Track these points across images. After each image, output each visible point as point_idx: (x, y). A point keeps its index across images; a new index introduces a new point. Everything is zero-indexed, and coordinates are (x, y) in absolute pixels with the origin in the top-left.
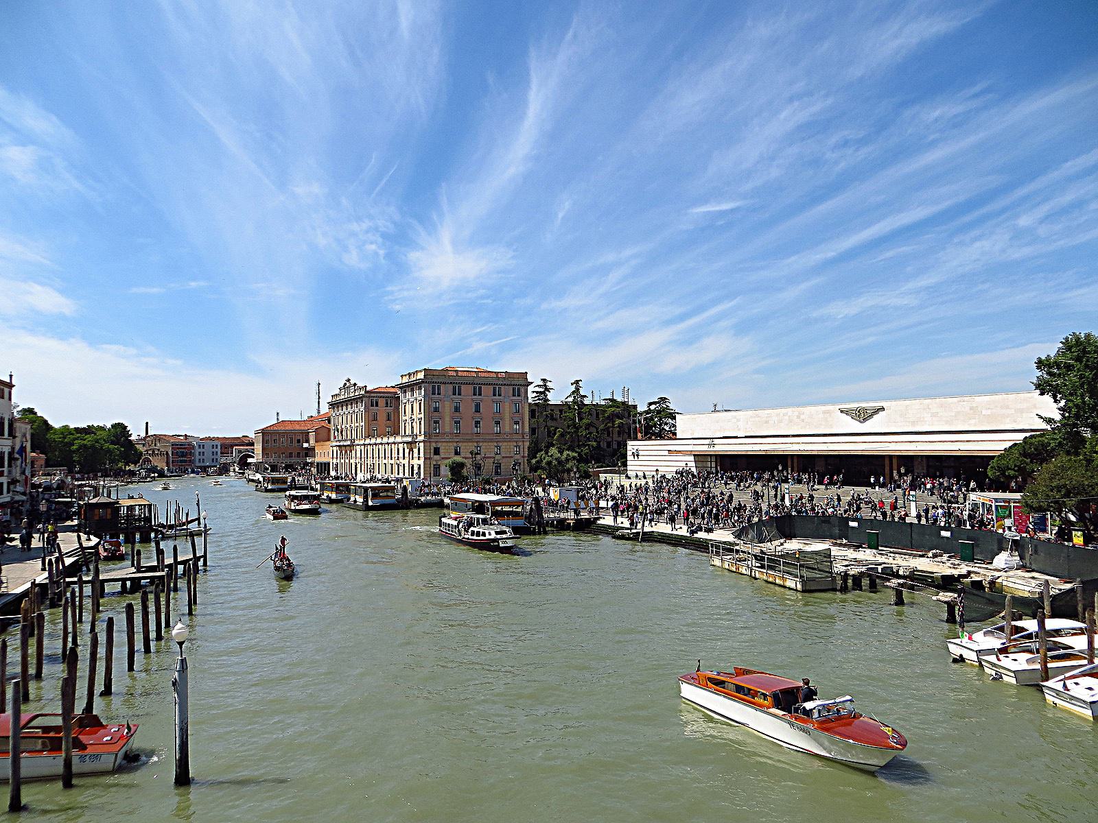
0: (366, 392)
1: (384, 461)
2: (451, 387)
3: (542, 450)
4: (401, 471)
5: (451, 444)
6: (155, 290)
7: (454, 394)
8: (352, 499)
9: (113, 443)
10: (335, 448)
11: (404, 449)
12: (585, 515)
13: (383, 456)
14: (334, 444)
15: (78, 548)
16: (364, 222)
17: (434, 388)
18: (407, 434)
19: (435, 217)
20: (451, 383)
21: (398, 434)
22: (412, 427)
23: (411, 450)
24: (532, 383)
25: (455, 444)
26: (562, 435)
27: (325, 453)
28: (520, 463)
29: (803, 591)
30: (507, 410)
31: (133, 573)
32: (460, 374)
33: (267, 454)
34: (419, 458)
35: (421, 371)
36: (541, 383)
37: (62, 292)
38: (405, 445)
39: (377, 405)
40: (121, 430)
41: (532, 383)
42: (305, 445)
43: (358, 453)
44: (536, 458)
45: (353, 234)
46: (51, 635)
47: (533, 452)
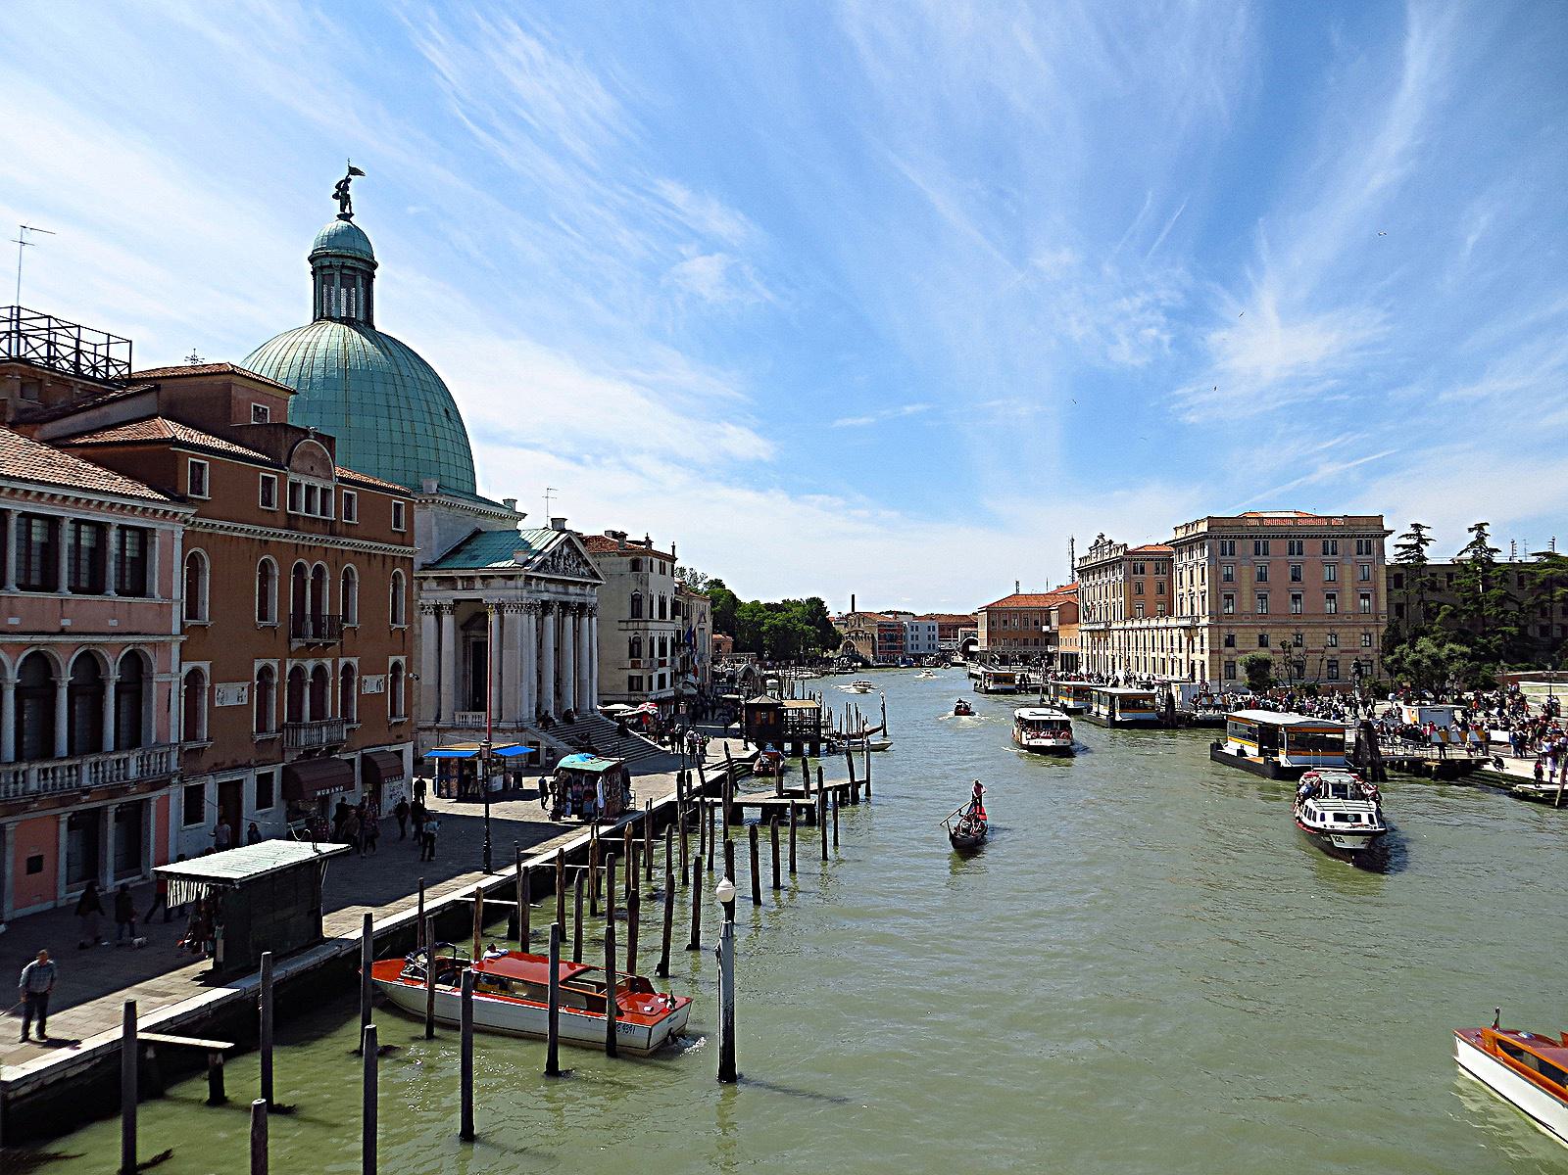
0: (1126, 553)
1: (1153, 655)
2: (1252, 542)
3: (1404, 642)
4: (1177, 669)
5: (1253, 630)
6: (863, 421)
7: (1257, 553)
8: (1095, 709)
9: (808, 623)
10: (1084, 633)
11: (1180, 638)
12: (1459, 754)
13: (1151, 646)
14: (1083, 627)
15: (724, 762)
16: (1138, 296)
17: (1223, 545)
18: (1184, 615)
19: (1249, 274)
20: (1251, 537)
21: (1171, 614)
22: (1192, 605)
23: (1191, 639)
24: (1391, 532)
25: (1259, 631)
26: (1452, 615)
27: (1072, 640)
28: (1372, 661)
30: (1348, 576)
31: (775, 798)
32: (1266, 522)
33: (994, 641)
35: (1203, 521)
36: (1412, 531)
37: (757, 431)
38: (1182, 630)
39: (1142, 572)
40: (817, 605)
41: (1391, 532)
42: (1046, 628)
43: (1116, 640)
44: (1393, 653)
45: (1123, 316)
46: (806, 856)
47: (1392, 641)
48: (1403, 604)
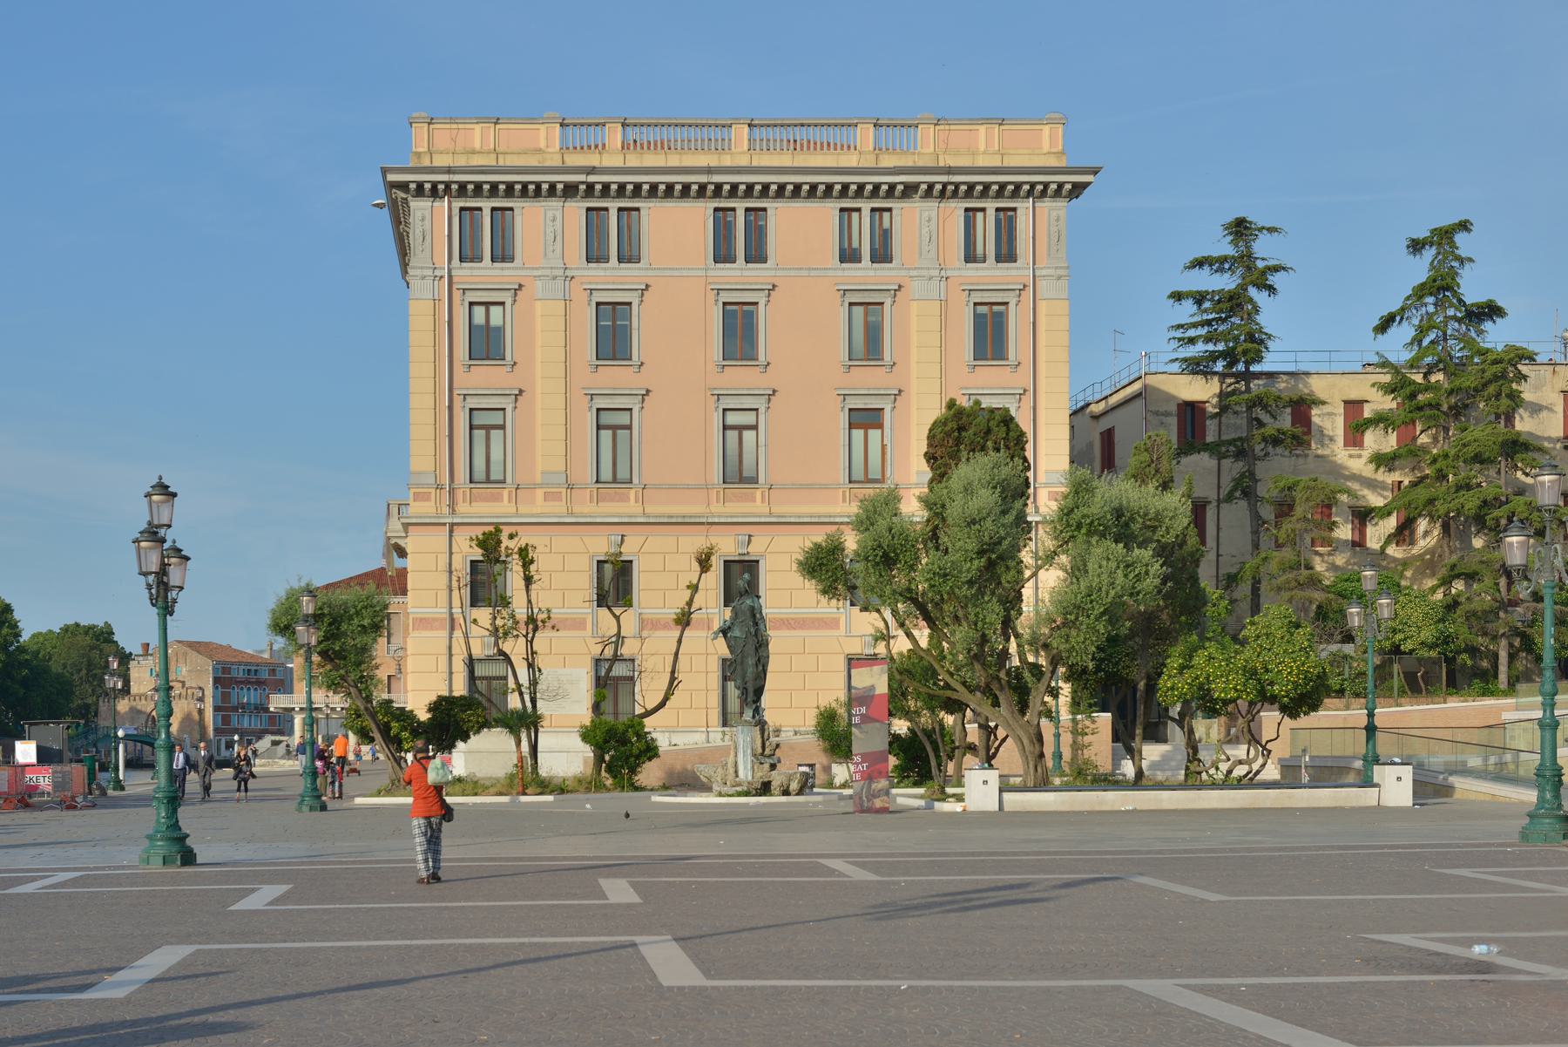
29: (968, 706)
36: (1225, 248)
48: (100, 771)
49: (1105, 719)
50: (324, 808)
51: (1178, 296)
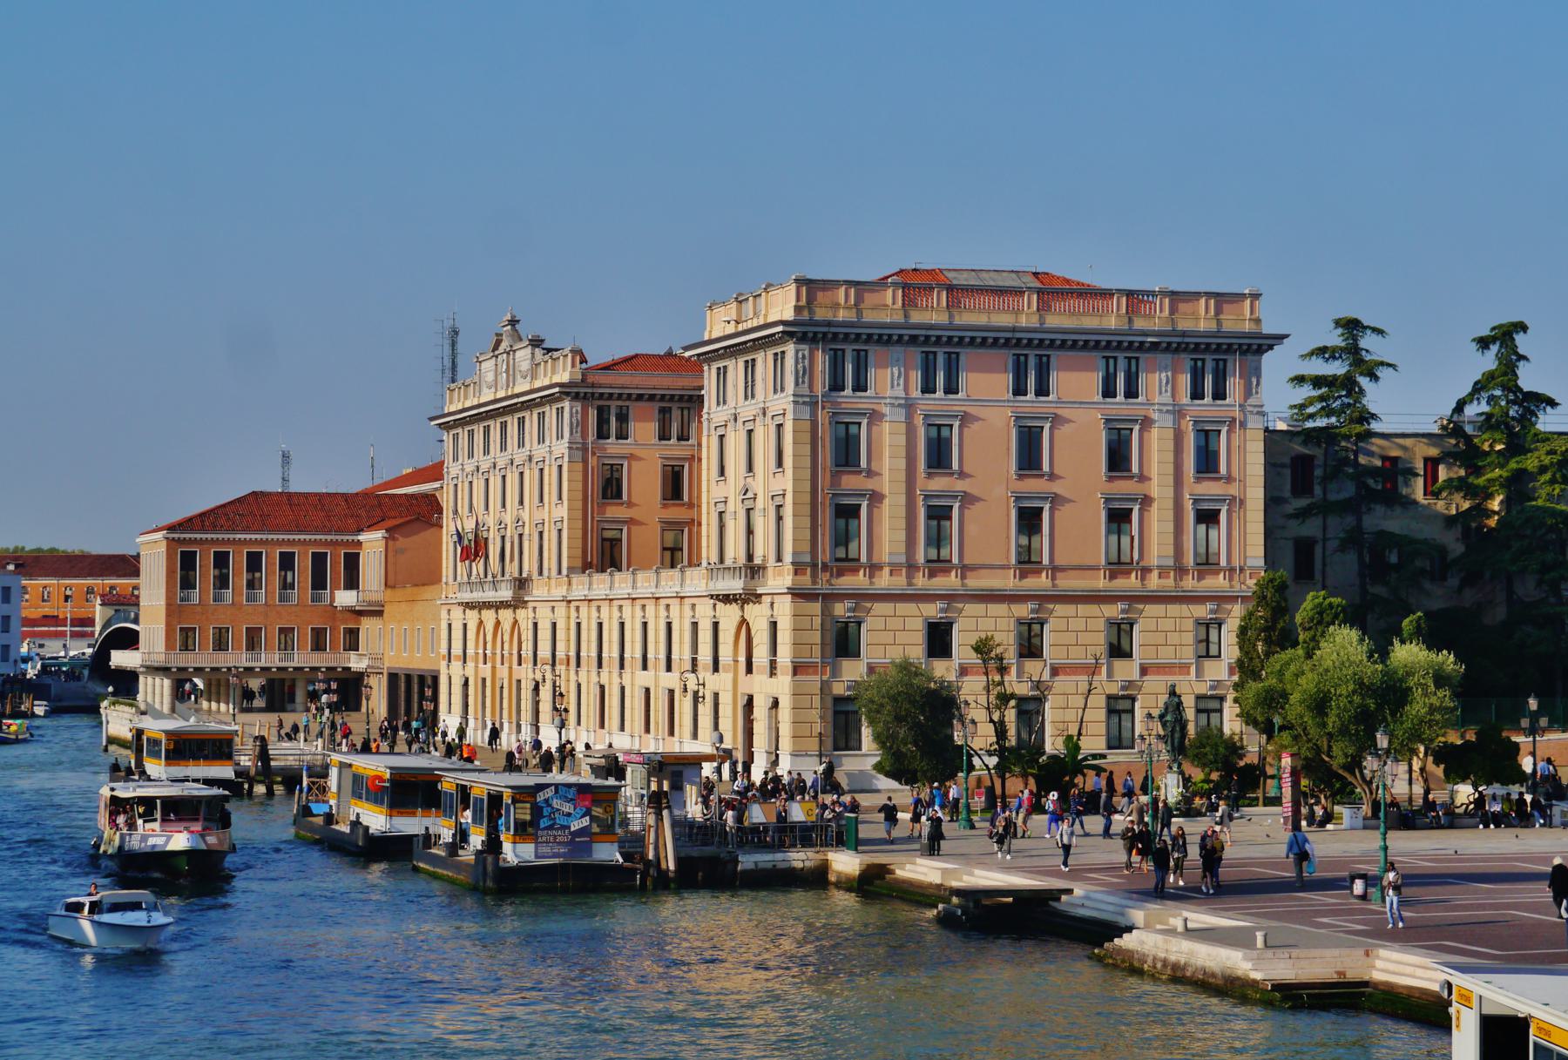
18: (728, 562)
34: (773, 669)
36: (1335, 339)
49: (1265, 736)
50: (973, 827)
51: (1300, 380)
